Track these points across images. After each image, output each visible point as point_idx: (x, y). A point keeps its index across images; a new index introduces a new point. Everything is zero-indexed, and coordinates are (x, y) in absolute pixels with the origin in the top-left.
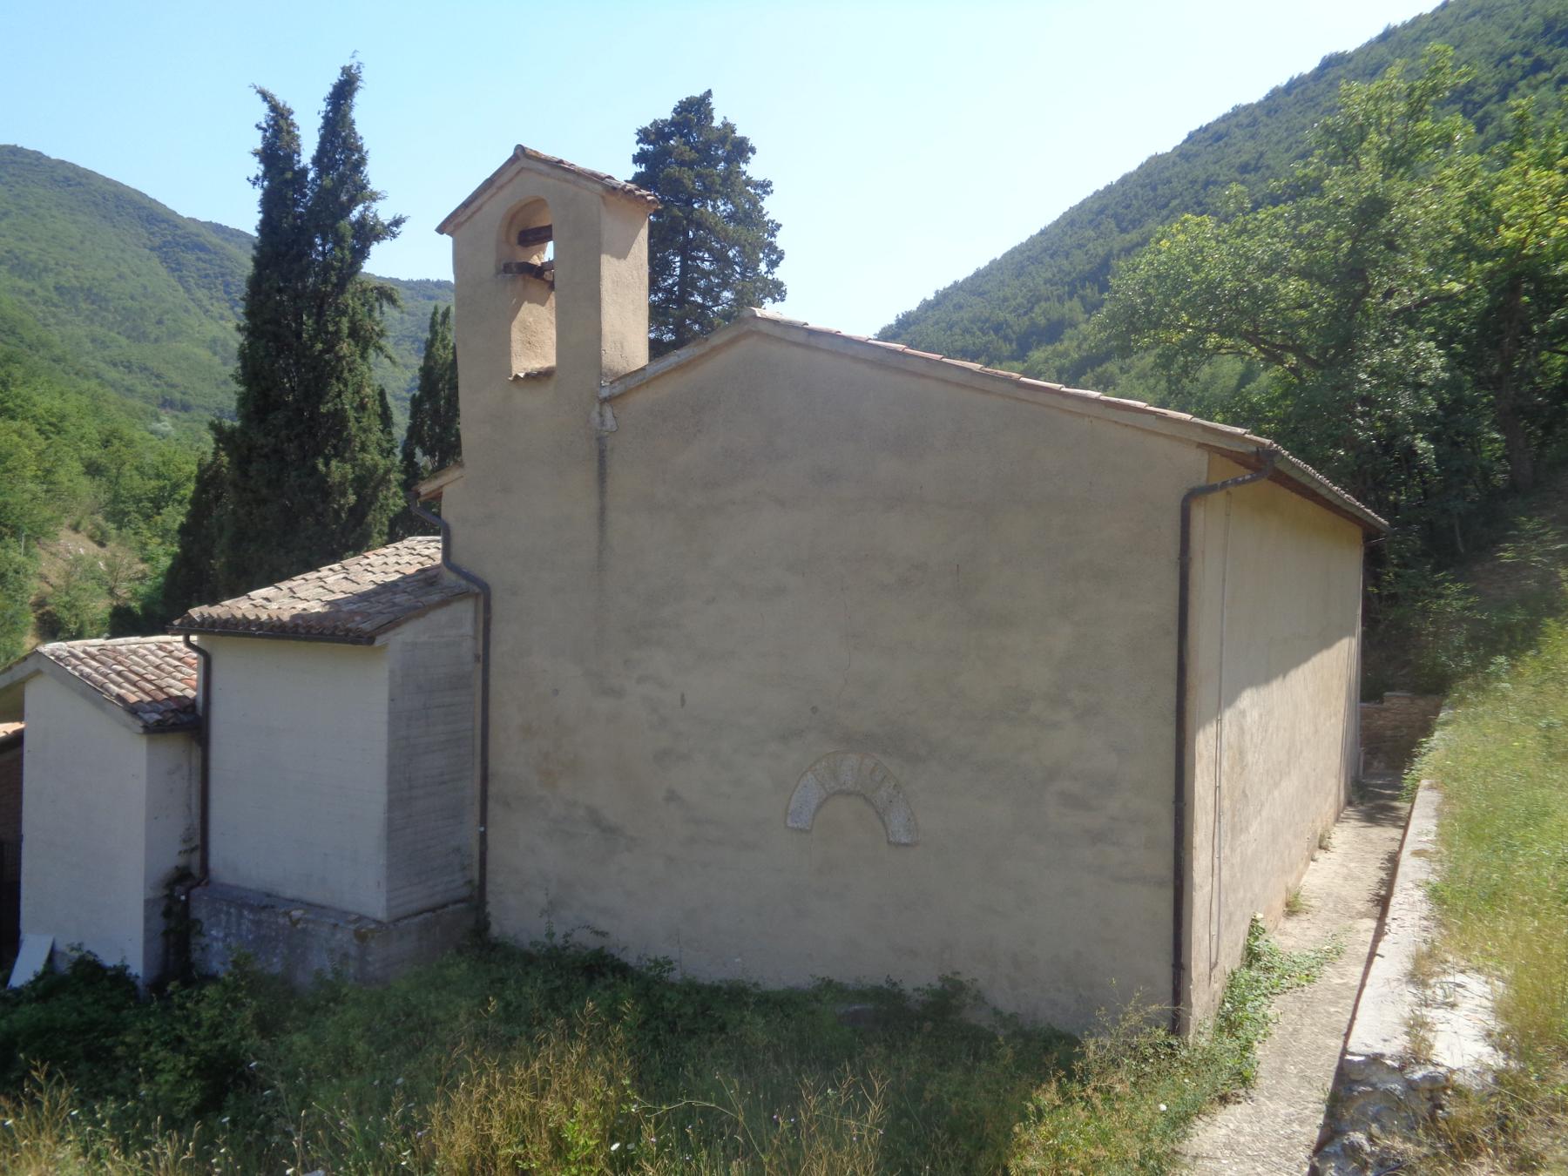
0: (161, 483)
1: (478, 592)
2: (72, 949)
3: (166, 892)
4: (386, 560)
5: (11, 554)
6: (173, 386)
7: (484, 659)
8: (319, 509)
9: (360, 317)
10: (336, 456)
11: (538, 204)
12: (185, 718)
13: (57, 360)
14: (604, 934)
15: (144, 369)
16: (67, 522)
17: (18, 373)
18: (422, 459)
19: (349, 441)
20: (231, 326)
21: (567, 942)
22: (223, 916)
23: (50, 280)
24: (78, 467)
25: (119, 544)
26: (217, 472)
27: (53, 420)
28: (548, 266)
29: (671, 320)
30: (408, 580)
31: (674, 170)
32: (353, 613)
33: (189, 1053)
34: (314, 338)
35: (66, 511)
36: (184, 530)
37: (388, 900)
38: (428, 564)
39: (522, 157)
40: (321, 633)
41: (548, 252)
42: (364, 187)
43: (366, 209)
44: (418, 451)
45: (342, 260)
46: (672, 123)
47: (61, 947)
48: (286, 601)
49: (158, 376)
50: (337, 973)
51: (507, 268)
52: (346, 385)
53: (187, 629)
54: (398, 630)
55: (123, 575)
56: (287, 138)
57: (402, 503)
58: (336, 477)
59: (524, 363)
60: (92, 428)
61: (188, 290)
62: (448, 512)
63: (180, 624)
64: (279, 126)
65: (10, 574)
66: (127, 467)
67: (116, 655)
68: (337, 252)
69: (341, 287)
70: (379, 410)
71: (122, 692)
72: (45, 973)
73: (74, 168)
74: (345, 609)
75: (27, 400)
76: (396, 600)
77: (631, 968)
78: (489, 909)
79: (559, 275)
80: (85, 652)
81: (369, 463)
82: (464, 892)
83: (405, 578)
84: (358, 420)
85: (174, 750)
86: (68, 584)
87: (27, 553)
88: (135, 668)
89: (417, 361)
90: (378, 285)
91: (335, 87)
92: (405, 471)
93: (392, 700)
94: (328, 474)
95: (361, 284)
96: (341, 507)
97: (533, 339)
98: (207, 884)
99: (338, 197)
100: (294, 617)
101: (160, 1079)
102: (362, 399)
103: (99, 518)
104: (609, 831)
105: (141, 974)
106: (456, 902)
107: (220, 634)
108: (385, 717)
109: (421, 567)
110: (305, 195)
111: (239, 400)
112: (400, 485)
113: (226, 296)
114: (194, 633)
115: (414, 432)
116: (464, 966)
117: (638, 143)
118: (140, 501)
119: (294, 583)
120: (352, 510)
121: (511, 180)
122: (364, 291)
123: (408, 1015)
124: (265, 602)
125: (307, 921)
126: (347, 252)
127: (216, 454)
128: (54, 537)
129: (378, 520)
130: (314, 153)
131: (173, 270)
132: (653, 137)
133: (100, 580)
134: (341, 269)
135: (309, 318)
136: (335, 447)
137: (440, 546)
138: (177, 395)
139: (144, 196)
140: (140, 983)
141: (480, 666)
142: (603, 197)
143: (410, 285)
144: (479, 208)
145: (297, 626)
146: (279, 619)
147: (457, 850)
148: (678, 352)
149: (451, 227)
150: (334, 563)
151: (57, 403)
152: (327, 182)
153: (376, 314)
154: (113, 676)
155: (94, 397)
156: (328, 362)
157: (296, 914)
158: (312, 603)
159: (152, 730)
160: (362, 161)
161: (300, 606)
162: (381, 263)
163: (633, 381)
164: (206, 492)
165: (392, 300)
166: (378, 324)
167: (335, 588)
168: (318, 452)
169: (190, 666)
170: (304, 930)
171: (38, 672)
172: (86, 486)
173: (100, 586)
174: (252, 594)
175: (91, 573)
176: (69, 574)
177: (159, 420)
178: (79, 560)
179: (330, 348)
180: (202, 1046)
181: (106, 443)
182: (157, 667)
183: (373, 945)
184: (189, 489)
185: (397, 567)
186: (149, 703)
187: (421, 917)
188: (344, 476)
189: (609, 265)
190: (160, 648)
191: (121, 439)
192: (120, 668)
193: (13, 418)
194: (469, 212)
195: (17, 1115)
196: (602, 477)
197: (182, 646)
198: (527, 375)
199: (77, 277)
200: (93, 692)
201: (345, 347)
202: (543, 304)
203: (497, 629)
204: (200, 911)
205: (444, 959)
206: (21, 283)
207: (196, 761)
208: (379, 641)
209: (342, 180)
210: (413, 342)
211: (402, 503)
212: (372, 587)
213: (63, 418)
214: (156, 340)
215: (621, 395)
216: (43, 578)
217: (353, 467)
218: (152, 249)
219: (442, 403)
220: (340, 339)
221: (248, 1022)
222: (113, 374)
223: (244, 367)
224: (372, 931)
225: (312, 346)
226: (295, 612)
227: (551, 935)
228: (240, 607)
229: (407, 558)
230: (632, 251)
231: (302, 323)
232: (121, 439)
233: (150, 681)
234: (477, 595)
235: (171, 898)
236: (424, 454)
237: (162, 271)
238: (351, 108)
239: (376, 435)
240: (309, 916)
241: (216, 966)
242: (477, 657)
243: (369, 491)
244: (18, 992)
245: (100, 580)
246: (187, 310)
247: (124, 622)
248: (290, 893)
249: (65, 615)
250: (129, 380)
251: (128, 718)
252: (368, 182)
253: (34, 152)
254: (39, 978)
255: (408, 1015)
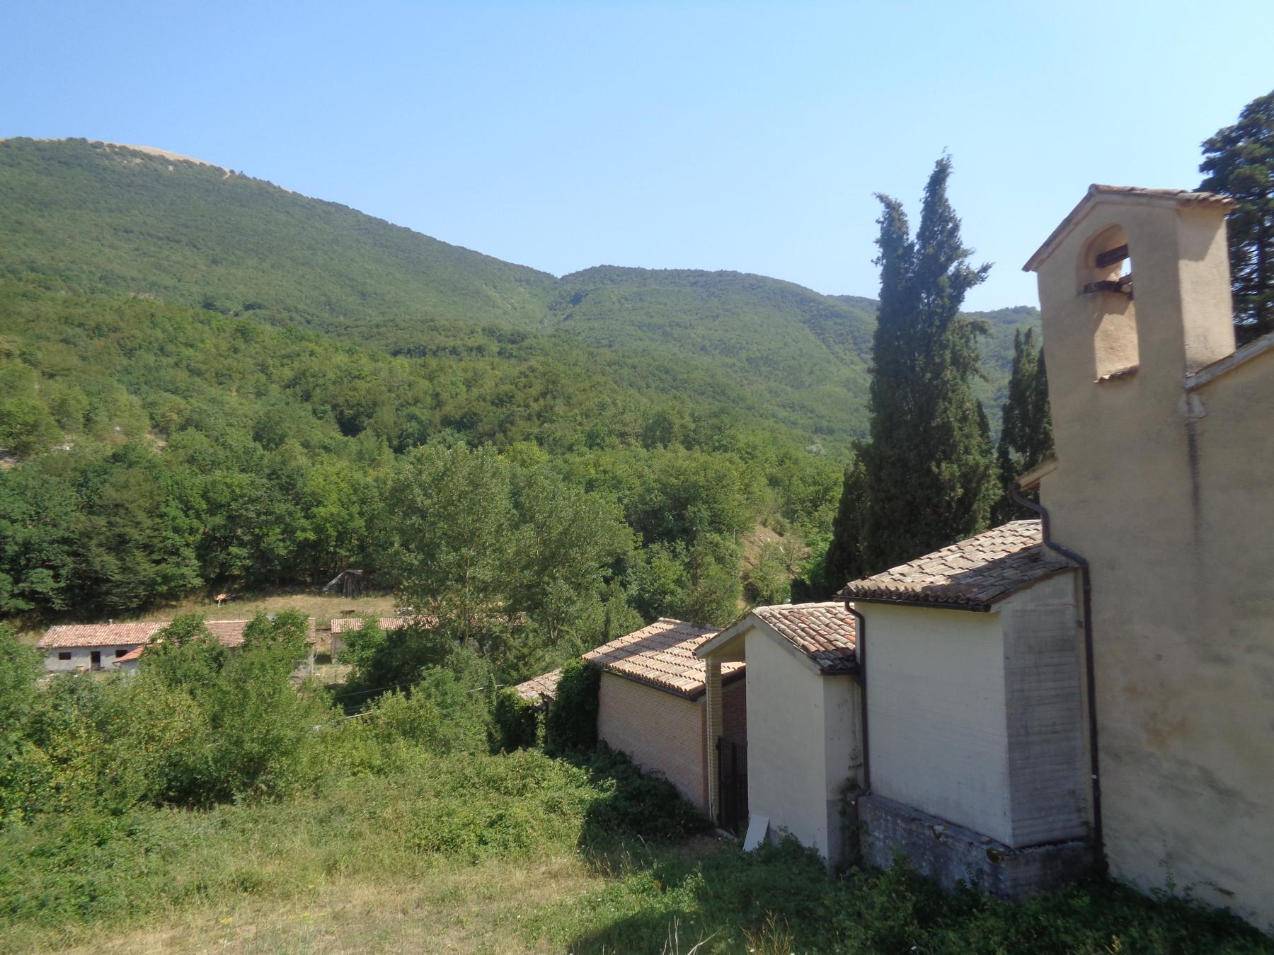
0: (817, 488)
1: (1079, 568)
2: (781, 830)
3: (841, 797)
4: (993, 541)
5: (728, 543)
6: (822, 417)
7: (1087, 625)
8: (935, 500)
9: (958, 348)
10: (945, 459)
11: (1115, 229)
12: (849, 665)
13: (749, 408)
14: (1229, 894)
15: (802, 407)
16: (759, 519)
17: (727, 419)
18: (1014, 456)
19: (954, 446)
20: (860, 367)
21: (1188, 895)
22: (882, 821)
23: (743, 355)
24: (764, 481)
25: (792, 534)
26: (858, 478)
27: (749, 450)
28: (1127, 279)
29: (1251, 306)
30: (1014, 557)
31: (1246, 170)
32: (970, 585)
33: (867, 927)
34: (924, 370)
35: (759, 512)
36: (837, 522)
37: (1014, 829)
38: (1030, 543)
39: (1095, 191)
40: (946, 601)
41: (1126, 268)
42: (958, 248)
43: (960, 264)
44: (1011, 450)
45: (943, 307)
46: (1240, 127)
47: (774, 827)
48: (918, 575)
49: (812, 412)
50: (975, 884)
51: (1087, 289)
52: (950, 403)
53: (848, 597)
54: (1009, 599)
55: (795, 556)
56: (898, 224)
57: (1000, 492)
58: (946, 475)
59: (1105, 369)
60: (772, 455)
61: (829, 347)
62: (1045, 501)
63: (842, 594)
64: (893, 216)
65: (727, 557)
66: (795, 478)
67: (800, 617)
68: (939, 301)
69: (943, 327)
70: (978, 420)
71: (806, 643)
72: (765, 844)
73: (755, 277)
74: (964, 582)
75: (733, 437)
76: (1005, 575)
77: (1262, 935)
78: (1106, 850)
79: (1137, 285)
80: (780, 613)
81: (971, 462)
82: (1081, 831)
83: (1011, 555)
84: (961, 429)
85: (842, 687)
86: (761, 563)
87: (737, 543)
88: (813, 626)
89: (1007, 378)
90: (971, 320)
91: (932, 178)
92: (1002, 467)
93: (1007, 658)
94: (940, 473)
95: (959, 322)
96: (952, 499)
97: (1115, 344)
98: (870, 794)
99: (939, 259)
100: (924, 588)
101: (848, 942)
102: (964, 412)
103: (779, 516)
104: (1226, 794)
105: (827, 857)
106: (1073, 840)
107: (870, 601)
108: (1002, 672)
109: (1023, 546)
110: (912, 263)
111: (872, 424)
112: (998, 478)
113: (855, 347)
114: (853, 600)
115: (1008, 436)
116: (1087, 899)
117: (1204, 153)
118: (804, 502)
119: (922, 562)
120: (960, 501)
121: (1087, 215)
122: (961, 327)
123: (1040, 934)
124: (901, 577)
125: (947, 836)
126: (946, 300)
127: (856, 465)
128: (752, 530)
129: (982, 508)
130: (918, 230)
131: (818, 334)
132: (1219, 145)
133: (781, 561)
134: (942, 314)
135: (920, 355)
136: (944, 452)
137: (1040, 527)
138: (824, 424)
139: (798, 286)
140: (826, 863)
141: (1082, 631)
142: (1177, 211)
143: (993, 315)
144: (1060, 244)
145: (927, 596)
146: (913, 590)
147: (1072, 793)
148: (1268, 336)
149: (1035, 265)
150: (950, 545)
151: (751, 438)
152: (930, 250)
153: (972, 343)
154: (799, 631)
155: (772, 431)
156: (936, 387)
157: (939, 828)
158: (937, 577)
159: (827, 672)
160: (956, 228)
161: (929, 579)
162: (974, 302)
163: (1221, 369)
164: (851, 493)
165: (983, 330)
166: (973, 352)
167: (954, 565)
168: (931, 456)
169: (850, 625)
170: (945, 843)
171: (753, 627)
172: (769, 493)
173: (781, 564)
174: (891, 570)
175: (775, 556)
176: (762, 556)
177: (813, 443)
178: (767, 546)
179: (937, 375)
180: (877, 924)
181: (781, 463)
182: (827, 625)
183: (1003, 865)
184: (838, 492)
185: (1004, 547)
186: (823, 652)
187: (1047, 847)
188: (952, 474)
189: (1188, 270)
190: (828, 612)
191: (790, 459)
192: (803, 626)
193: (725, 451)
194: (1050, 249)
195: (758, 947)
196: (1194, 458)
197: (842, 610)
198: (1113, 377)
199: (759, 350)
200: (786, 642)
201: (948, 374)
202: (1122, 313)
203: (1095, 597)
204: (866, 815)
205: (1069, 889)
206: (727, 360)
207: (858, 699)
208: (994, 608)
209: (940, 246)
210: (997, 360)
211: (1000, 492)
212: (984, 563)
213: (755, 448)
214: (810, 386)
215: (1208, 383)
216: (747, 559)
217: (959, 466)
218: (804, 322)
219: (1030, 407)
220: (945, 368)
221: (909, 912)
222: (783, 414)
223: (874, 398)
224: (1001, 853)
225: (923, 376)
226: (925, 584)
227: (1171, 885)
228: (882, 581)
229: (1011, 539)
230: (1210, 251)
231: (915, 360)
232: (790, 459)
233: (822, 636)
234: (1075, 570)
235: (844, 801)
236: (1017, 451)
237: (812, 337)
238: (944, 191)
239: (976, 440)
240: (949, 832)
241: (879, 860)
242: (1079, 624)
243: (974, 485)
244: (750, 854)
245: (781, 561)
246: (829, 362)
247: (802, 592)
248: (933, 811)
249: (760, 585)
250: (793, 417)
251: (810, 662)
252: (961, 244)
253: (733, 272)
254: (762, 847)
255: (1040, 934)
